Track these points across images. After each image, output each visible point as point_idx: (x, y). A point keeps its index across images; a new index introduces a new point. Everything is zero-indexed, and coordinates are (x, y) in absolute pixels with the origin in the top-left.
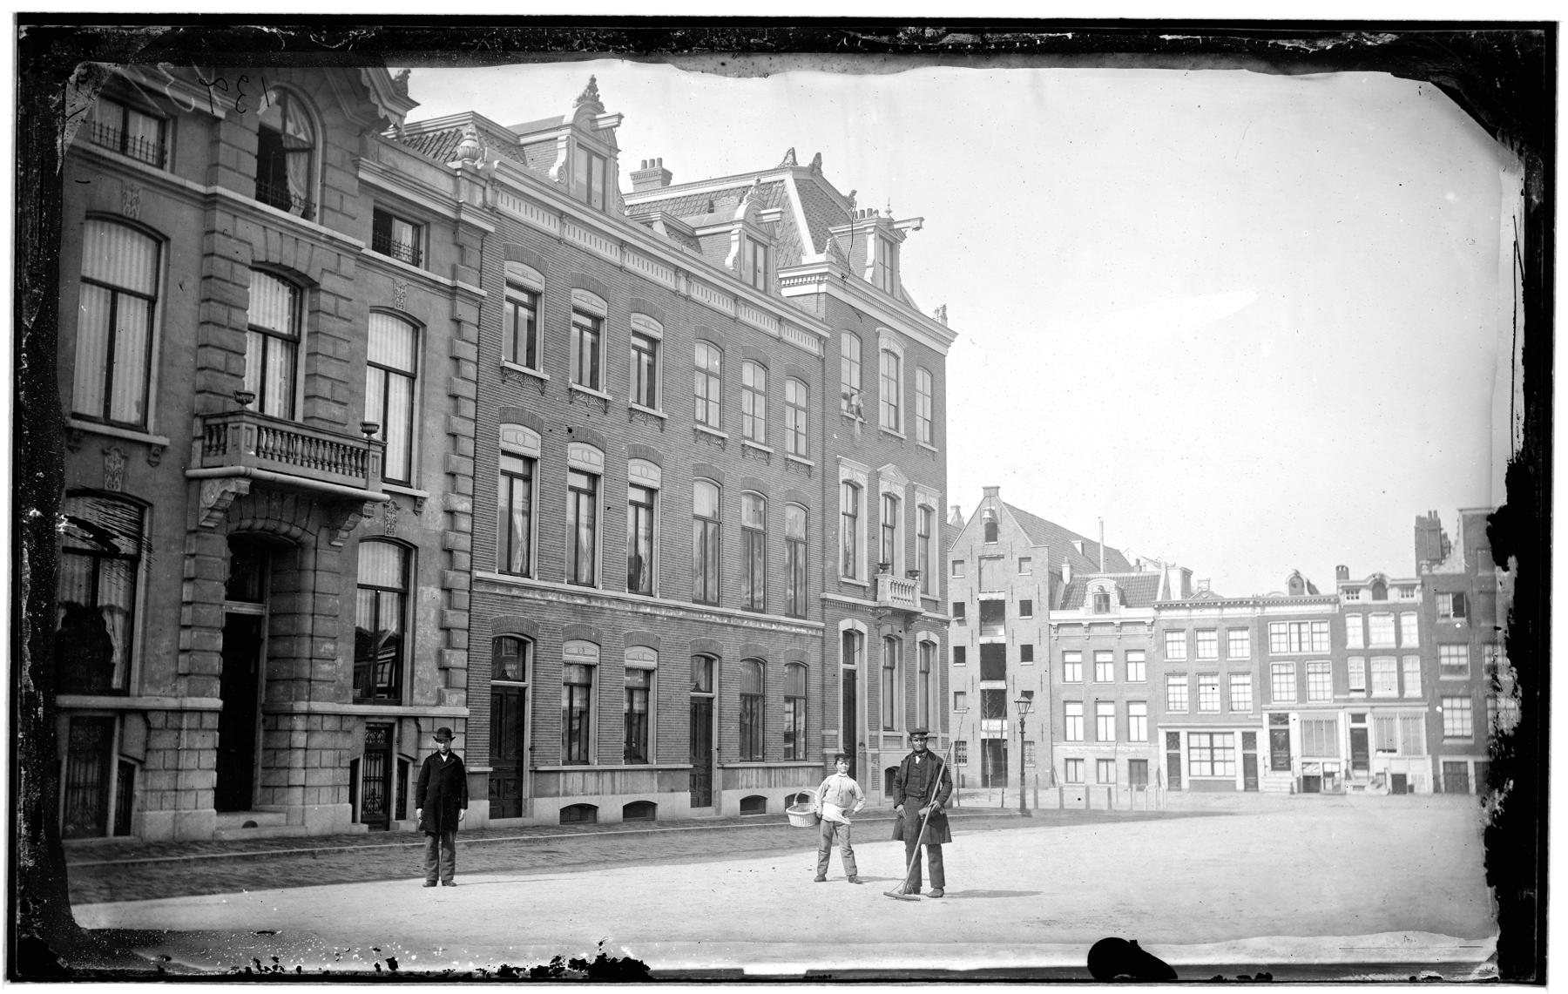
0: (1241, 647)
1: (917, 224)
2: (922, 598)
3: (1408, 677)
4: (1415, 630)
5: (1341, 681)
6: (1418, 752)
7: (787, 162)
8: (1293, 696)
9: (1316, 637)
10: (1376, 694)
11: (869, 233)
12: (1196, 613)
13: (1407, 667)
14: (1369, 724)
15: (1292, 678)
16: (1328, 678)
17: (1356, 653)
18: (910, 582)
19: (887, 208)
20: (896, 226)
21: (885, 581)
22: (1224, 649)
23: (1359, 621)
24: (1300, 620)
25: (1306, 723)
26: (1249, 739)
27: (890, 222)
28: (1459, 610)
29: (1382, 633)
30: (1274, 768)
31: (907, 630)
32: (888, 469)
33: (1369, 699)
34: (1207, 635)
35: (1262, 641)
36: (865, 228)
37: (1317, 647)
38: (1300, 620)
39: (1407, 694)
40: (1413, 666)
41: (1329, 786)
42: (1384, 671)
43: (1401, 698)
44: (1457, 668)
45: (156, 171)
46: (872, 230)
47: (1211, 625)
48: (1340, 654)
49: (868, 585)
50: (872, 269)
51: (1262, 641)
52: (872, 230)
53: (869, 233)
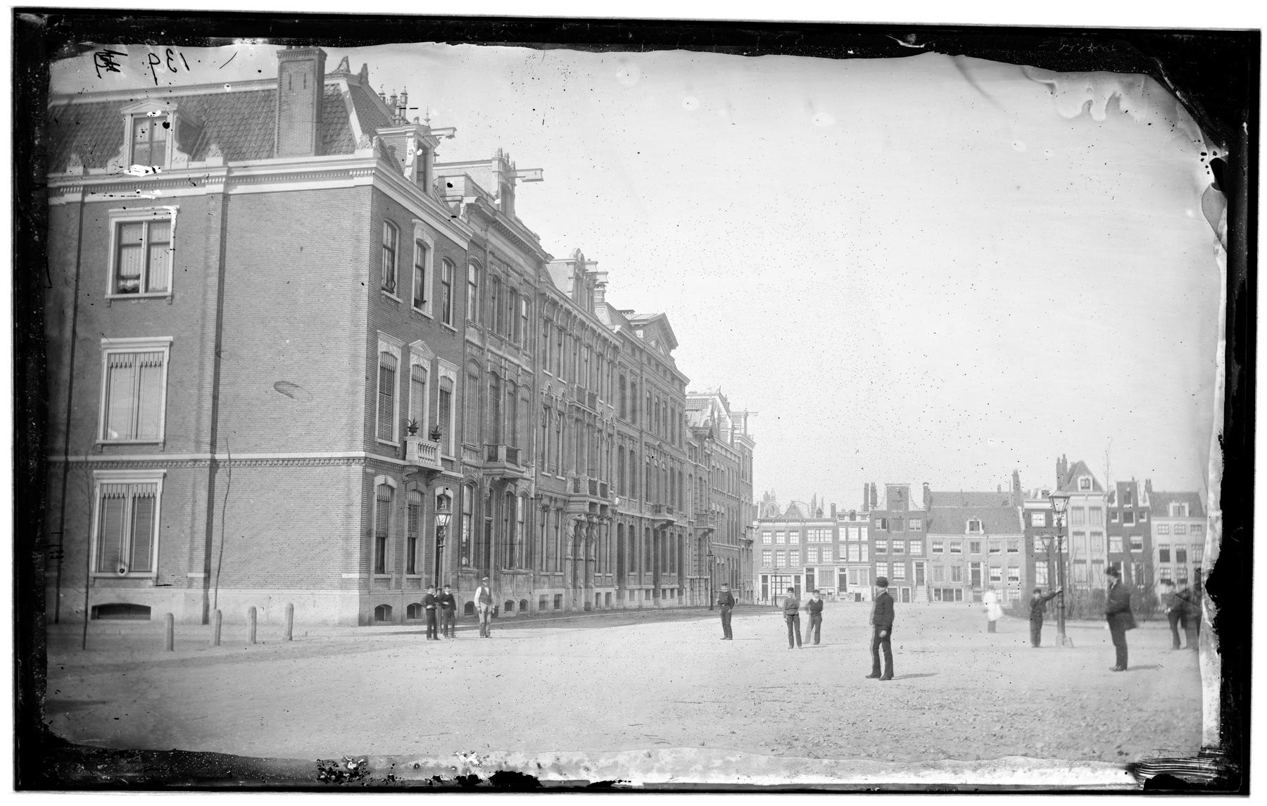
0: (795, 539)
1: (450, 132)
2: (442, 459)
3: (863, 553)
4: (867, 534)
5: (836, 555)
6: (866, 584)
7: (341, 68)
8: (816, 560)
9: (826, 536)
10: (850, 560)
11: (409, 137)
12: (777, 524)
13: (862, 529)
14: (847, 572)
15: (816, 553)
16: (831, 553)
17: (843, 543)
18: (432, 444)
19: (425, 117)
20: (433, 133)
21: (413, 444)
22: (788, 540)
23: (844, 529)
24: (819, 528)
25: (821, 572)
26: (797, 579)
27: (428, 129)
28: (884, 526)
29: (854, 534)
30: (807, 591)
31: (427, 485)
32: (417, 344)
33: (847, 562)
34: (781, 534)
35: (804, 538)
36: (406, 132)
37: (826, 540)
38: (819, 528)
39: (863, 560)
40: (865, 548)
41: (830, 598)
42: (854, 550)
43: (860, 562)
44: (207, 575)
45: (173, 222)
46: (412, 134)
47: (783, 529)
48: (836, 541)
49: (399, 445)
50: (411, 169)
51: (804, 538)
52: (412, 134)
53: (409, 137)
